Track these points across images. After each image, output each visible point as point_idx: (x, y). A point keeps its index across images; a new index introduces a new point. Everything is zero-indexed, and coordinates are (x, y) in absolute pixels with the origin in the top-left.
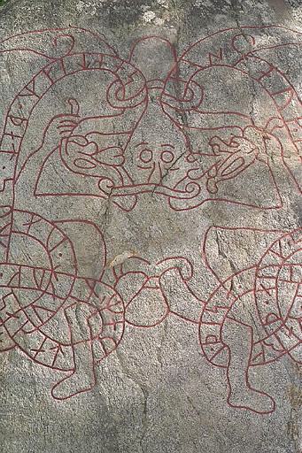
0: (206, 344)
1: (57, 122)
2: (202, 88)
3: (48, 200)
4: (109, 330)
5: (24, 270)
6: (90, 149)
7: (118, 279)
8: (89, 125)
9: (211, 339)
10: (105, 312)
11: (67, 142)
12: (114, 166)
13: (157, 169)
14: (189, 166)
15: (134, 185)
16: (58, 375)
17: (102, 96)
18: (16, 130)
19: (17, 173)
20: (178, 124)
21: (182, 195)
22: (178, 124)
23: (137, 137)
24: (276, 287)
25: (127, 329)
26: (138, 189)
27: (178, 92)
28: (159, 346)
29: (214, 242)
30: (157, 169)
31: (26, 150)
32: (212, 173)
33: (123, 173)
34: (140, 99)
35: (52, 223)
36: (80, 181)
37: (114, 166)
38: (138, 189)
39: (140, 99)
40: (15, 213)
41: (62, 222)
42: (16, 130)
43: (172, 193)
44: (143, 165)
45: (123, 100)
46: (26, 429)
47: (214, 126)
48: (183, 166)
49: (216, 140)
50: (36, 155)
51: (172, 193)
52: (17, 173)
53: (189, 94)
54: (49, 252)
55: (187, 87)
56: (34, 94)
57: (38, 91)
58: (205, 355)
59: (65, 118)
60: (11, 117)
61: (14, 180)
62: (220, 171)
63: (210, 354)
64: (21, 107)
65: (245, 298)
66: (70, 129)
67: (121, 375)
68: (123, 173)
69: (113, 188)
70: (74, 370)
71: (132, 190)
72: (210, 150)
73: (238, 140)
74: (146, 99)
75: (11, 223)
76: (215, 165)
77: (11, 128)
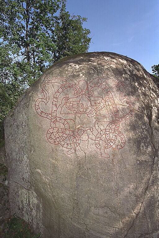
1: (64, 99)
3: (63, 115)
6: (71, 105)
8: (71, 100)
9: (97, 144)
10: (76, 138)
17: (73, 94)
20: (89, 100)
21: (90, 114)
22: (89, 100)
23: (81, 102)
25: (81, 142)
32: (96, 110)
34: (81, 94)
39: (81, 94)
43: (88, 114)
48: (90, 108)
51: (88, 114)
63: (97, 147)
69: (76, 112)
71: (80, 113)
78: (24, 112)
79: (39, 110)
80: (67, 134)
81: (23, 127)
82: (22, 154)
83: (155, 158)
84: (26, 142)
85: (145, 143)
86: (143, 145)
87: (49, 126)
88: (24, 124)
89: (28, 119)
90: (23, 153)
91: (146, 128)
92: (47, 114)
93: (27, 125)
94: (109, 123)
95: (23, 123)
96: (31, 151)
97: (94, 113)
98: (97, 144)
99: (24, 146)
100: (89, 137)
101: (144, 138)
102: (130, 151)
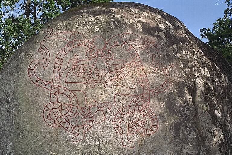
0: (116, 128)
2: (113, 52)
4: (88, 123)
5: (62, 104)
6: (81, 70)
7: (90, 107)
11: (75, 67)
12: (89, 75)
13: (101, 76)
14: (110, 75)
15: (94, 80)
16: (74, 135)
18: (59, 63)
19: (60, 76)
21: (107, 84)
23: (95, 66)
24: (135, 112)
26: (95, 81)
27: (106, 53)
28: (103, 128)
29: (117, 98)
30: (101, 76)
31: (62, 69)
33: (91, 77)
34: (96, 55)
35: (71, 91)
36: (79, 78)
37: (89, 75)
38: (95, 81)
39: (96, 55)
40: (60, 87)
41: (74, 90)
42: (59, 63)
44: (96, 74)
45: (91, 55)
46: (65, 150)
47: (116, 64)
49: (117, 68)
50: (65, 70)
52: (60, 76)
53: (109, 54)
54: (70, 99)
55: (109, 52)
56: (65, 52)
57: (66, 51)
58: (116, 131)
59: (74, 60)
60: (58, 58)
61: (59, 78)
62: (118, 77)
63: (117, 131)
64: (61, 56)
65: (126, 115)
66: (75, 63)
67: (92, 136)
68: (91, 77)
70: (78, 134)
71: (94, 82)
72: (115, 71)
73: (123, 68)
74: (97, 55)
75: (59, 90)
76: (117, 75)
77: (58, 62)
78: (11, 79)
79: (34, 76)
80: (73, 111)
81: (8, 102)
82: (4, 143)
83: (200, 149)
84: (11, 125)
85: (186, 127)
86: (184, 130)
87: (48, 100)
88: (11, 96)
89: (17, 90)
90: (7, 140)
91: (188, 106)
92: (45, 82)
93: (16, 97)
94: (135, 97)
95: (9, 95)
96: (18, 138)
97: (114, 83)
98: (118, 126)
99: (9, 131)
100: (106, 117)
101: (185, 119)
102: (164, 138)
